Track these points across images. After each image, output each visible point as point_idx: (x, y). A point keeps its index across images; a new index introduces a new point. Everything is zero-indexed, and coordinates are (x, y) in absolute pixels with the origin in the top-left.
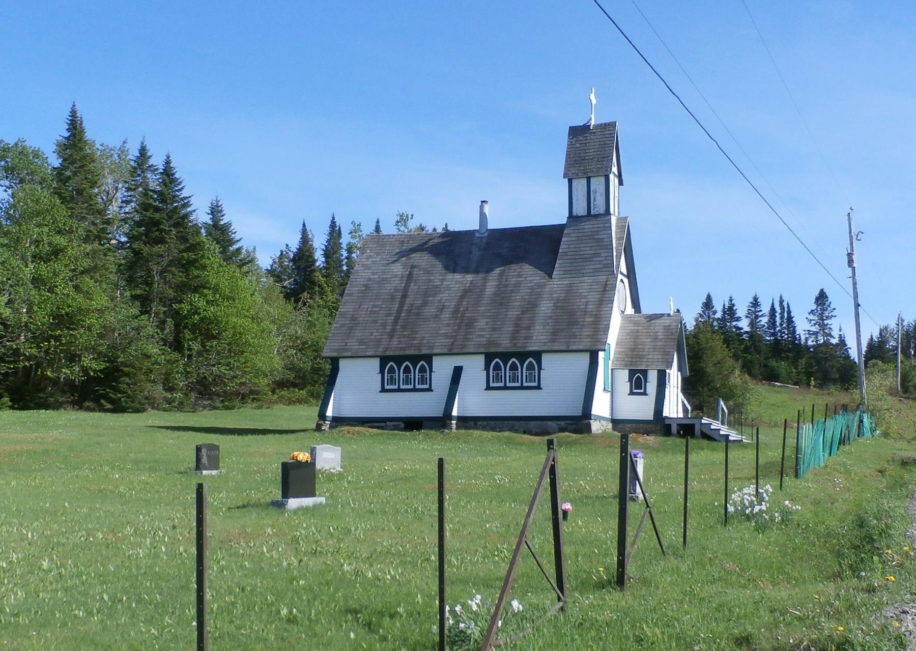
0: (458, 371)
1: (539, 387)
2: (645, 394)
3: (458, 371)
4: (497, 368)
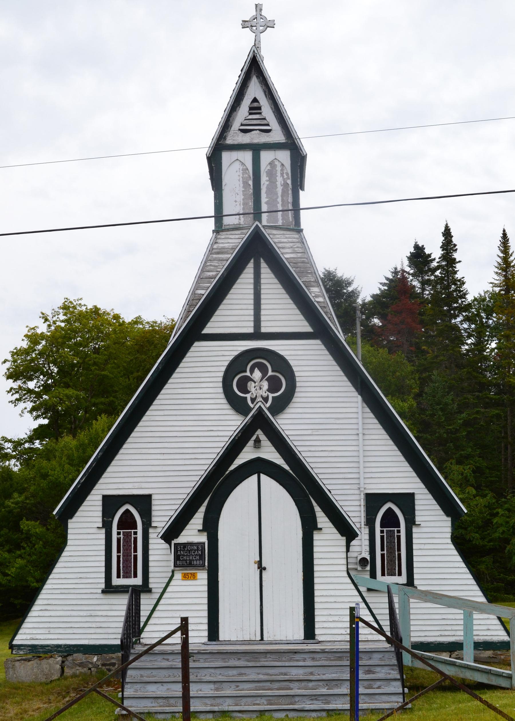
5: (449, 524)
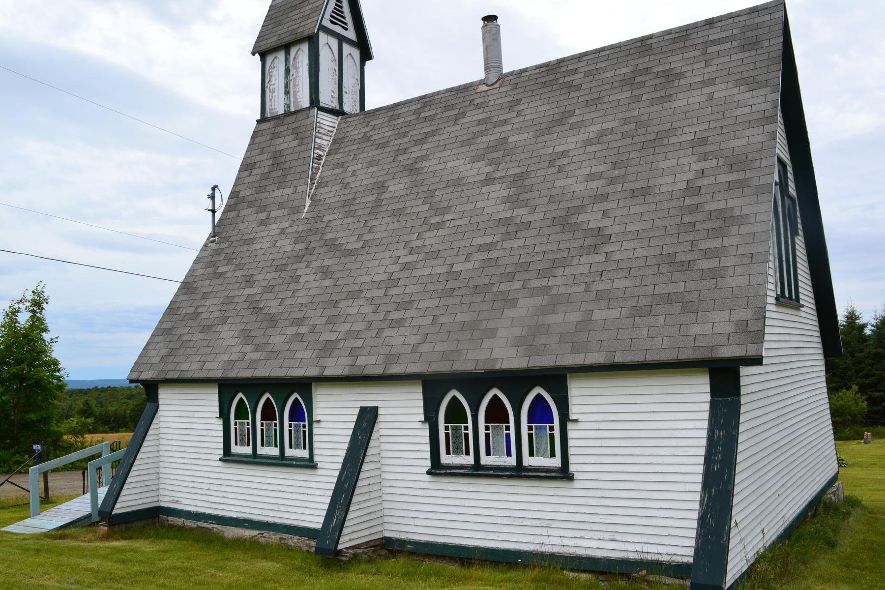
0: (368, 418)
1: (564, 474)
2: (309, 464)
3: (368, 418)
4: (455, 414)
5: (427, 427)
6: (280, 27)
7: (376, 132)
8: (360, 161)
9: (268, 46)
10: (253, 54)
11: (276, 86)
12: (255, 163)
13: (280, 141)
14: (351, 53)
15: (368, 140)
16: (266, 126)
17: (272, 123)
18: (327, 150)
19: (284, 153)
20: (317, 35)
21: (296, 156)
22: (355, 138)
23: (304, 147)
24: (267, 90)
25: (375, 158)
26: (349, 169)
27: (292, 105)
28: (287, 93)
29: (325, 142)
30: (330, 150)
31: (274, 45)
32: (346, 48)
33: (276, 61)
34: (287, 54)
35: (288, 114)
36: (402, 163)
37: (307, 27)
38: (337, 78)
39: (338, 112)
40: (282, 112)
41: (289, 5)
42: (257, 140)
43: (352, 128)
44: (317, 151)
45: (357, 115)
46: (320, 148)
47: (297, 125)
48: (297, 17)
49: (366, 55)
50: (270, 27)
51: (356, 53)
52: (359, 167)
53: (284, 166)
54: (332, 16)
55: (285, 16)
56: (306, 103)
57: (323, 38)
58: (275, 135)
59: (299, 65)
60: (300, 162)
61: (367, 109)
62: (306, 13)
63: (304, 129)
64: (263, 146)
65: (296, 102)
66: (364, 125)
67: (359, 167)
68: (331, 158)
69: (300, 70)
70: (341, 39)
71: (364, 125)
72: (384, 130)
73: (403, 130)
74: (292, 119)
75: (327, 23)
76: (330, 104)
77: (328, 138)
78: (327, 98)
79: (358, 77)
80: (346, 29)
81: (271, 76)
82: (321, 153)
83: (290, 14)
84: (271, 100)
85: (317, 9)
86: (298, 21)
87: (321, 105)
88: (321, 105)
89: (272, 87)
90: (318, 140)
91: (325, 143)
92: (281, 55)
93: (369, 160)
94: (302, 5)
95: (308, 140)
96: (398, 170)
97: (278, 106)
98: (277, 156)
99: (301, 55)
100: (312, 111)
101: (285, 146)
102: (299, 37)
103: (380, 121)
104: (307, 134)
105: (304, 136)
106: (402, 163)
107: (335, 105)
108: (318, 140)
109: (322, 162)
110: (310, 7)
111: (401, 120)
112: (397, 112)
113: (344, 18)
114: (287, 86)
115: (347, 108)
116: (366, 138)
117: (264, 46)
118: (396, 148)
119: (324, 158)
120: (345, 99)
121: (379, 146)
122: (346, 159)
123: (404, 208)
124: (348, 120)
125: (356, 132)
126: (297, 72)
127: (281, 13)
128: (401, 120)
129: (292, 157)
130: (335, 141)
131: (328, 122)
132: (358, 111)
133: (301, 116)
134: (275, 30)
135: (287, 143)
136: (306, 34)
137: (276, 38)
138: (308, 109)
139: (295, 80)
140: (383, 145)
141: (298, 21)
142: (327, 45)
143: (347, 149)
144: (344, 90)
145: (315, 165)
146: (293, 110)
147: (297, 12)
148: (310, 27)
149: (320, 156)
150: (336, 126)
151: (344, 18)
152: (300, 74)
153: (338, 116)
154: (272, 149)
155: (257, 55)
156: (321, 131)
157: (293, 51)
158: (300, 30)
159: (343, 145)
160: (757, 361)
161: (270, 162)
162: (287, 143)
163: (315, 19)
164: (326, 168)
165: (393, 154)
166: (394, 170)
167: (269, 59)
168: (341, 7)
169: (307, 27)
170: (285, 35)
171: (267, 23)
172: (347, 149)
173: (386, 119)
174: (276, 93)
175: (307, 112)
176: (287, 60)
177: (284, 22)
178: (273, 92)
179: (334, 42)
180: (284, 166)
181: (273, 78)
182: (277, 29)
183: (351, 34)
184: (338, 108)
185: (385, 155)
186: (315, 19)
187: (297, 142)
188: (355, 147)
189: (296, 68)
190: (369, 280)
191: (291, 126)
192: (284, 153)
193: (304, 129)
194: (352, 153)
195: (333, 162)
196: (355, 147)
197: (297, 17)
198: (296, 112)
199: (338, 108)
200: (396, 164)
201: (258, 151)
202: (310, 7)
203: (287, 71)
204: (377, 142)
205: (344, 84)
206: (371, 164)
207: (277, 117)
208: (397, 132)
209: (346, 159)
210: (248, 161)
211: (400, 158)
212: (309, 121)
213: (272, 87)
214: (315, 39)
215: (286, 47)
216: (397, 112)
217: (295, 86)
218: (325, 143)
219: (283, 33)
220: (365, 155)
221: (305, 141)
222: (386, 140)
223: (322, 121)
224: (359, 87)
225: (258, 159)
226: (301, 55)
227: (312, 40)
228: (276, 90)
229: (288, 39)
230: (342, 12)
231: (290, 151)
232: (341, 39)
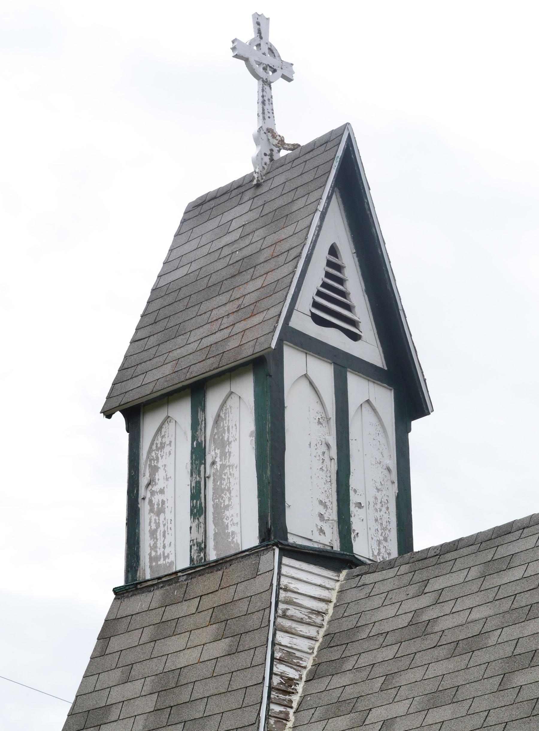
6: (180, 341)
7: (447, 608)
8: (403, 692)
9: (147, 390)
10: (108, 414)
11: (168, 496)
12: (108, 707)
13: (176, 643)
14: (369, 399)
15: (425, 634)
16: (138, 603)
17: (158, 594)
18: (309, 663)
19: (189, 676)
20: (278, 353)
21: (221, 684)
22: (386, 627)
23: (243, 659)
24: (144, 508)
25: (447, 683)
26: (374, 716)
27: (211, 544)
28: (198, 511)
29: (304, 644)
30: (317, 665)
31: (164, 386)
32: (358, 388)
33: (169, 429)
34: (198, 407)
35: (200, 568)
36: (526, 694)
37: (250, 336)
38: (334, 467)
39: (338, 560)
40: (183, 563)
41: (203, 284)
42: (115, 644)
43: (377, 601)
44: (280, 668)
45: (390, 565)
46: (290, 658)
47: (224, 596)
48: (222, 311)
49: (412, 402)
50: (153, 341)
51: (384, 399)
52: (401, 708)
53: (187, 714)
54: (316, 305)
55: (191, 313)
56: (249, 536)
57: (294, 362)
58: (166, 629)
59: (231, 435)
60: (234, 700)
61: (419, 545)
62: (247, 300)
63: (243, 607)
64: (130, 657)
65: (222, 533)
66: (412, 590)
67: (401, 708)
68: (320, 685)
69: (234, 448)
70: (343, 364)
71: (412, 590)
72: (468, 602)
73: (524, 600)
74: (210, 581)
75: (303, 323)
76: (317, 537)
77: (311, 631)
78: (307, 519)
79: (392, 462)
80: (355, 337)
81: (154, 470)
82: (292, 673)
83: (205, 306)
84: (153, 533)
85: (277, 288)
86: (226, 322)
87: (291, 539)
88: (291, 539)
89: (157, 499)
90: (283, 639)
91: (303, 644)
92: (182, 412)
93: (430, 687)
94: (238, 280)
95: (257, 638)
96: (516, 713)
97: (172, 547)
98: (169, 684)
99: (236, 409)
100: (266, 558)
101: (192, 656)
102: (227, 362)
103: (458, 578)
104: (254, 621)
105: (244, 629)
106: (526, 694)
107: (330, 539)
108: (283, 639)
109: (296, 699)
110: (258, 283)
111: (517, 573)
112: (502, 551)
113: (348, 307)
114: (196, 494)
115: (362, 548)
116: (419, 627)
117: (135, 393)
118: (508, 650)
119: (300, 688)
120: (356, 524)
121: (457, 649)
122: (364, 688)
123: (343, 659)
124: (368, 579)
125: (390, 611)
126: (224, 455)
127: (181, 306)
128: (517, 573)
129: (212, 687)
130: (330, 640)
131: (309, 584)
132: (395, 554)
133: (236, 572)
134: (164, 348)
135: (195, 649)
136: (248, 352)
137: (167, 369)
138: (253, 552)
139: (218, 477)
140: (466, 646)
141: (226, 322)
142: (305, 381)
143: (365, 660)
144: (354, 498)
145: (276, 708)
146: (212, 556)
147: (224, 298)
148: (255, 336)
149: (290, 681)
150: (333, 596)
151: (348, 307)
152: (233, 460)
153: (338, 570)
154: (156, 666)
155: (119, 418)
156: (292, 611)
157: (214, 400)
158: (233, 343)
159: (353, 649)
160: (117, 591)
161: (149, 704)
162: (195, 649)
163: (273, 312)
164: (306, 715)
165: (497, 668)
166: (505, 715)
167: (150, 425)
168: (341, 281)
169: (250, 336)
170: (192, 359)
171: (144, 333)
172: (365, 660)
173: (474, 573)
174: (169, 515)
175: (252, 561)
176: (196, 425)
177: (189, 325)
178: (160, 511)
179: (323, 373)
180: (187, 714)
181: (160, 475)
182: (169, 345)
183: (369, 349)
184: (337, 547)
185: (476, 673)
186: (273, 312)
187: (223, 646)
188: (389, 653)
189: (223, 444)
190: (419, 677)
191: (207, 602)
192: (189, 676)
193: (243, 607)
194: (379, 670)
195: (326, 699)
196: (389, 653)
197: (222, 311)
198: (221, 563)
199: (337, 547)
200: (509, 696)
201: (116, 675)
202: (258, 283)
203: (199, 454)
204: (449, 637)
205: (354, 482)
206: (434, 700)
207: (171, 579)
208: (506, 605)
209: (364, 688)
210: (90, 703)
211: (520, 679)
212: (258, 585)
213: (157, 499)
214: (271, 367)
215: (196, 390)
216: (502, 551)
217: (218, 492)
218: (303, 644)
219: (187, 357)
220: (418, 674)
221: (247, 641)
222: (476, 629)
223: (294, 585)
224: (394, 490)
225: (116, 695)
226: (236, 409)
227: (264, 368)
228: (169, 504)
229: (200, 370)
230: (343, 294)
231: (205, 670)
232: (343, 364)
